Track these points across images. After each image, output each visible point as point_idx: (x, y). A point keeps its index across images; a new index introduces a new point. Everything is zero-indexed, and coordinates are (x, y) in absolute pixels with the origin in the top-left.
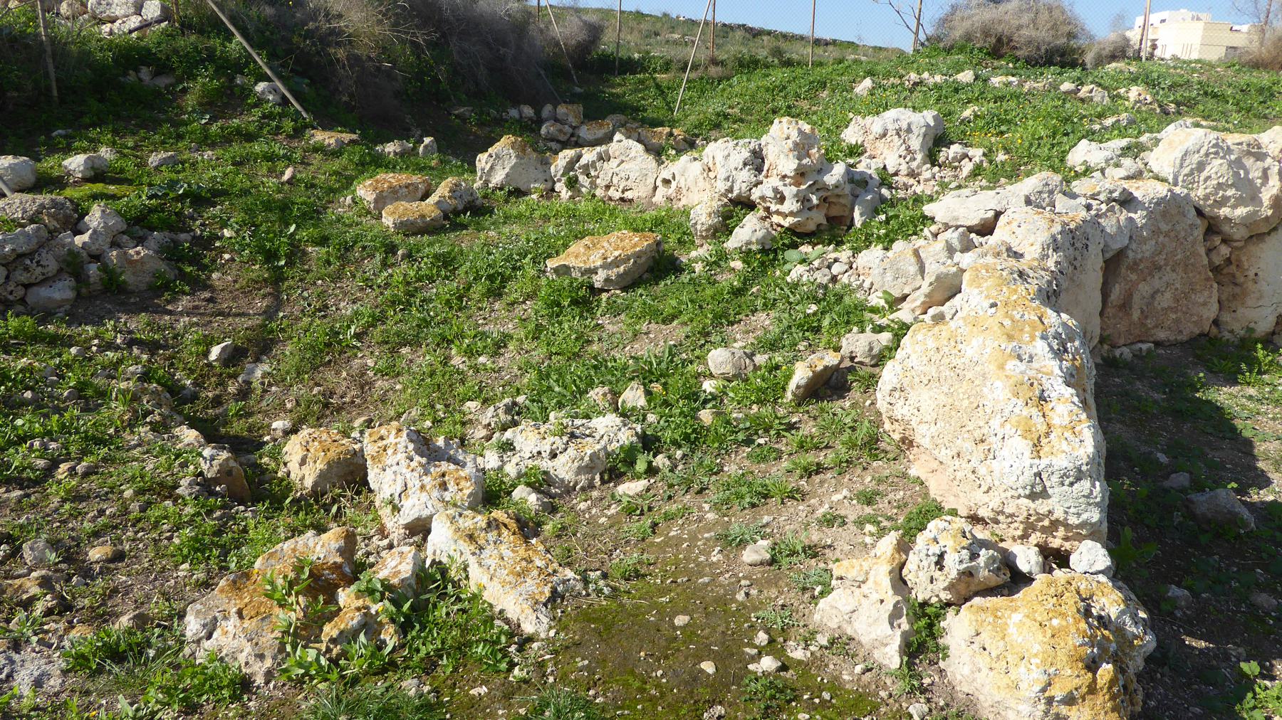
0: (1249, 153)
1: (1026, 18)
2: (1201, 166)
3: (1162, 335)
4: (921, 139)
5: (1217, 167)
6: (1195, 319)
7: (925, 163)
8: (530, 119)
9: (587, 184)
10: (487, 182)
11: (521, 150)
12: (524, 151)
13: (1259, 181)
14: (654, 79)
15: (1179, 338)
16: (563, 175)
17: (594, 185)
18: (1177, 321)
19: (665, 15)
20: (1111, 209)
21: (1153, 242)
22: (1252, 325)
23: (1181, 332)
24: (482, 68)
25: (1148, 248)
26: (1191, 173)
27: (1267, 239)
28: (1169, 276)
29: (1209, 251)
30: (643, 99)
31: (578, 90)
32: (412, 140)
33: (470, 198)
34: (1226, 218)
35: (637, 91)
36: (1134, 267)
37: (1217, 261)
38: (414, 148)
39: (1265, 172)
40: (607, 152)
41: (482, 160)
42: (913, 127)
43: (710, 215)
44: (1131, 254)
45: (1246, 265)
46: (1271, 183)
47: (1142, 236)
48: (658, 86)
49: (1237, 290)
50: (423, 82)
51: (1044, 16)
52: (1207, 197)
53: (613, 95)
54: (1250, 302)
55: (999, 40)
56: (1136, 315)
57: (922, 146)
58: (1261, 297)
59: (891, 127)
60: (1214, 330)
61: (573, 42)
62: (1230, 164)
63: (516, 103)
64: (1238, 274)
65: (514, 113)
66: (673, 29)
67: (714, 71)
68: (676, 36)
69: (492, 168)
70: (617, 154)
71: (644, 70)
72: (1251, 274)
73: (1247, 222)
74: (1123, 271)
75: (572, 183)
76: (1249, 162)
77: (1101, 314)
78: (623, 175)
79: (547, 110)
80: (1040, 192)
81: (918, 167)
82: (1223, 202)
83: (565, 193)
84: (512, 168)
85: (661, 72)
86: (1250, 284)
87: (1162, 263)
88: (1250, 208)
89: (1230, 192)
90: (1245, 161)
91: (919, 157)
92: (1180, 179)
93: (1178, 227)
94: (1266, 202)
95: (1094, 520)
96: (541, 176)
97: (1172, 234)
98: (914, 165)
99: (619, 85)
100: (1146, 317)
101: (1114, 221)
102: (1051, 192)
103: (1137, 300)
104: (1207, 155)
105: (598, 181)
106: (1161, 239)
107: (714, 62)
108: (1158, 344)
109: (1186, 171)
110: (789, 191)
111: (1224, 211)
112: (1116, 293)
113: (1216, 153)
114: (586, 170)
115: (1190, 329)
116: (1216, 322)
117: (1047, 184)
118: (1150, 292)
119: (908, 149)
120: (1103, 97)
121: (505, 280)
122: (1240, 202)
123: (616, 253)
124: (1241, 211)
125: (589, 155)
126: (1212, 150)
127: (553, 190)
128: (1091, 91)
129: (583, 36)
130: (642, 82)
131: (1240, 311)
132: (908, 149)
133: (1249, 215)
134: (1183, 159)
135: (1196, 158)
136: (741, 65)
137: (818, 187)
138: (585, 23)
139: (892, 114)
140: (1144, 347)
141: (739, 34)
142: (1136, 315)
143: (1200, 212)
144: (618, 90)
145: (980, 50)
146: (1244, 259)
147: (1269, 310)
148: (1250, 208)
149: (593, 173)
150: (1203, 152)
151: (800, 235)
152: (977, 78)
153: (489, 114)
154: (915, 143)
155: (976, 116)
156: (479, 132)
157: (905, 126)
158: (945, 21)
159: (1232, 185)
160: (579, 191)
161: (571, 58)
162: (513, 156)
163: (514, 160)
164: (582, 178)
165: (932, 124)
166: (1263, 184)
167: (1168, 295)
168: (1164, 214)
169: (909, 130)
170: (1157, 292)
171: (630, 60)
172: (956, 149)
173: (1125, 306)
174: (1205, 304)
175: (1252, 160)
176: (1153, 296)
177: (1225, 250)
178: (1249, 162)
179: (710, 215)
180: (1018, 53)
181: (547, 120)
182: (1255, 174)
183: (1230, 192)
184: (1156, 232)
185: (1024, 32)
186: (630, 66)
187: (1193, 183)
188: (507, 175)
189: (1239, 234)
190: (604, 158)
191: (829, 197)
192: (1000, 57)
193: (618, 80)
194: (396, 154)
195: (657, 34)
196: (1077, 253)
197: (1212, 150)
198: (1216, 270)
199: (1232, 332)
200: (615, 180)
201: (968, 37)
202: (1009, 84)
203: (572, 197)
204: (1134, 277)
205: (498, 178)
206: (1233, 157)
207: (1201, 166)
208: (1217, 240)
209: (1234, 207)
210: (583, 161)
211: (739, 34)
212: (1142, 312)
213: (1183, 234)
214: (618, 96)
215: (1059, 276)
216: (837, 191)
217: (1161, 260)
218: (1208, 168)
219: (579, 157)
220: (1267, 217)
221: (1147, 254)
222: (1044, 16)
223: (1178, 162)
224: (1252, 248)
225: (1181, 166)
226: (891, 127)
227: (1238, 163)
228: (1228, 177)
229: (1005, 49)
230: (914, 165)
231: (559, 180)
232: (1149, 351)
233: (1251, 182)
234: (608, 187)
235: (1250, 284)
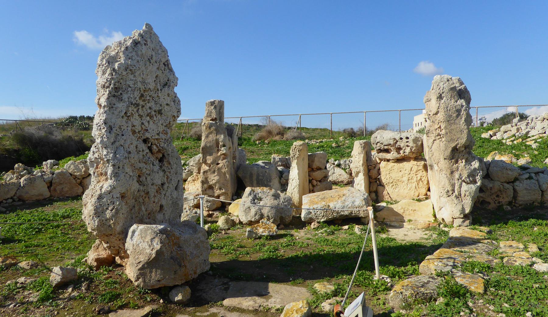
2: (70, 167)
29: (76, 181)
36: (54, 184)
73: (81, 175)
82: (75, 172)
142: (59, 192)
143: (71, 175)
154: (48, 166)
176: (63, 188)
207: (70, 167)
217: (62, 182)
224: (85, 180)
227: (77, 165)
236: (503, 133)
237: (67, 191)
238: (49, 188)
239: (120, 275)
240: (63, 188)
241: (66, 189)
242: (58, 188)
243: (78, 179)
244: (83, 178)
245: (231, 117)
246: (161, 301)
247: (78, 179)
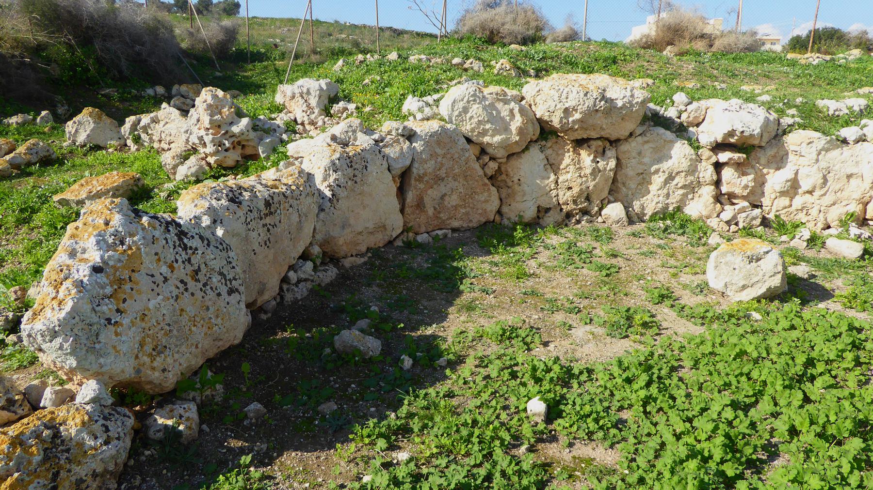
0: (498, 100)
1: (509, 18)
2: (465, 110)
3: (456, 224)
4: (317, 99)
5: (476, 109)
6: (480, 211)
7: (321, 115)
8: (163, 95)
9: (147, 140)
10: (74, 142)
11: (98, 120)
12: (100, 118)
13: (508, 118)
14: (274, 65)
15: (471, 225)
16: (130, 134)
17: (151, 141)
18: (467, 214)
19: (336, 22)
20: (397, 141)
21: (433, 162)
22: (522, 214)
23: (471, 221)
24: (123, 60)
25: (430, 166)
26: (460, 115)
27: (523, 155)
28: (453, 184)
29: (483, 166)
30: (265, 79)
31: (218, 74)
32: (32, 113)
33: (47, 154)
34: (488, 143)
35: (262, 73)
36: (420, 179)
37: (490, 172)
38: (35, 119)
39: (511, 111)
40: (157, 117)
41: (70, 127)
42: (311, 91)
43: (173, 158)
44: (415, 171)
45: (512, 174)
46: (516, 118)
47: (422, 158)
48: (276, 70)
49: (510, 191)
50: (75, 71)
51: (521, 17)
52: (473, 130)
53: (244, 77)
54: (518, 198)
55: (492, 32)
56: (431, 212)
57: (318, 103)
58: (524, 195)
59: (297, 91)
60: (498, 218)
61: (215, 41)
62: (484, 108)
63: (153, 85)
64: (508, 180)
65: (150, 92)
66: (341, 31)
67: (314, 58)
68: (343, 36)
69: (76, 131)
70: (163, 117)
71: (268, 59)
72: (516, 179)
73: (504, 145)
74: (413, 182)
75: (137, 140)
76: (499, 105)
77: (402, 211)
78: (167, 132)
79: (176, 88)
80: (347, 132)
81: (316, 118)
82: (484, 133)
83: (133, 147)
84: (91, 131)
85: (280, 60)
86: (516, 186)
87: (444, 175)
88: (504, 136)
89: (488, 126)
90: (497, 104)
91: (316, 111)
92: (454, 119)
93: (452, 151)
94: (514, 132)
95: (74, 365)
96: (116, 136)
97: (449, 156)
98: (313, 117)
99: (251, 70)
100: (439, 213)
101: (398, 148)
102: (354, 131)
103: (427, 200)
104: (468, 102)
105: (154, 138)
106: (440, 159)
107: (315, 52)
108: (454, 230)
109: (456, 113)
110: (208, 139)
111: (487, 139)
112: (410, 196)
113: (474, 100)
114: (145, 129)
115: (476, 219)
116: (499, 212)
117: (350, 126)
118: (439, 195)
119: (308, 106)
120: (479, 67)
121: (34, 211)
122: (496, 132)
123: (99, 188)
124: (497, 139)
125: (145, 119)
126: (471, 99)
127: (126, 145)
128: (471, 63)
129: (221, 37)
130: (266, 67)
131: (513, 204)
132: (308, 106)
133: (503, 141)
134: (453, 106)
135: (461, 105)
136: (333, 54)
137: (228, 134)
138: (222, 27)
139: (301, 82)
140: (440, 232)
141: (387, 34)
142: (431, 212)
143: (469, 140)
144: (249, 74)
145: (480, 39)
146: (510, 170)
147: (531, 203)
148: (504, 136)
149: (150, 132)
150: (465, 100)
151: (225, 169)
152: (400, 56)
153: (130, 93)
154: (313, 102)
155: (372, 82)
156: (121, 106)
157: (305, 91)
158: (462, 20)
159: (488, 121)
160: (143, 145)
161: (215, 52)
162: (91, 122)
163: (92, 125)
164: (143, 136)
165: (325, 88)
166: (511, 120)
167: (454, 197)
168: (439, 143)
169: (308, 93)
170: (445, 195)
171: (258, 52)
172: (342, 104)
173: (420, 205)
174: (486, 201)
175: (501, 104)
176: (443, 197)
177: (493, 165)
178: (499, 105)
179: (173, 158)
180: (505, 41)
181: (175, 96)
182: (505, 113)
183: (488, 126)
184: (433, 155)
185: (507, 27)
186: (258, 57)
187: (462, 121)
188: (88, 136)
189: (501, 154)
190: (155, 121)
191: (239, 143)
192: (493, 44)
193: (250, 66)
194: (17, 123)
195: (330, 35)
196: (356, 172)
197: (471, 99)
198: (491, 178)
199: (509, 219)
200: (163, 136)
201: (472, 31)
202: (420, 60)
203: (138, 150)
204: (422, 186)
205: (81, 138)
206: (487, 103)
207: (465, 110)
208: (486, 158)
209: (493, 136)
210: (142, 124)
211: (387, 34)
212: (435, 209)
213: (456, 156)
214: (247, 77)
215: (336, 189)
216: (243, 137)
217: (442, 173)
218: (471, 111)
219: (139, 121)
220: (516, 141)
221: (430, 170)
222: (521, 17)
223: (450, 107)
224: (514, 162)
225: (453, 111)
226: (297, 91)
227: (492, 106)
228: (484, 116)
229: (495, 39)
230: (313, 117)
231: (128, 138)
232: (445, 236)
233: (503, 119)
234: (160, 141)
235: (516, 186)
236: (314, 243)
237: (456, 207)
238: (401, 192)
239: (823, 316)
240: (443, 197)
241: (453, 200)
242: (432, 196)
243: (493, 159)
244: (510, 156)
245: (608, 95)
246: (333, 326)
247: (493, 159)
